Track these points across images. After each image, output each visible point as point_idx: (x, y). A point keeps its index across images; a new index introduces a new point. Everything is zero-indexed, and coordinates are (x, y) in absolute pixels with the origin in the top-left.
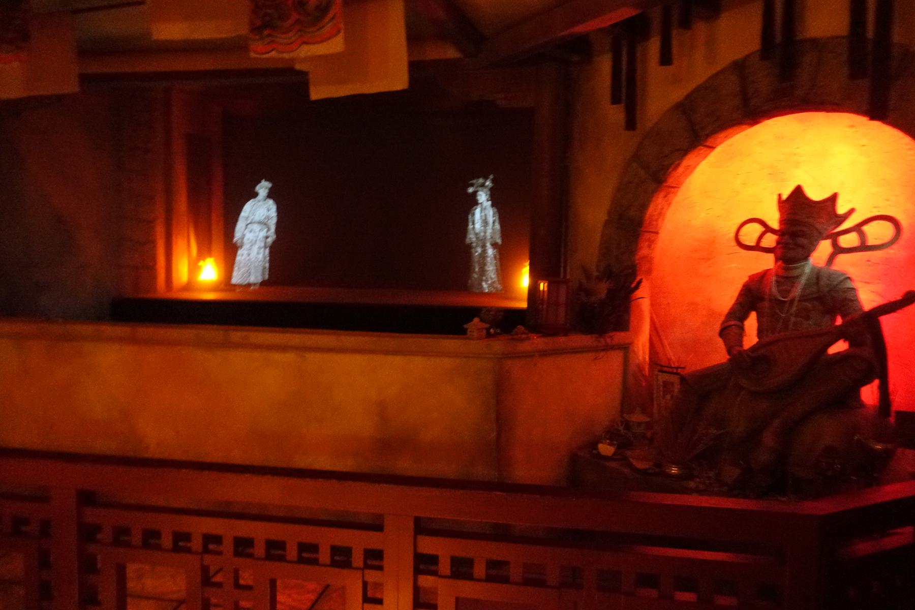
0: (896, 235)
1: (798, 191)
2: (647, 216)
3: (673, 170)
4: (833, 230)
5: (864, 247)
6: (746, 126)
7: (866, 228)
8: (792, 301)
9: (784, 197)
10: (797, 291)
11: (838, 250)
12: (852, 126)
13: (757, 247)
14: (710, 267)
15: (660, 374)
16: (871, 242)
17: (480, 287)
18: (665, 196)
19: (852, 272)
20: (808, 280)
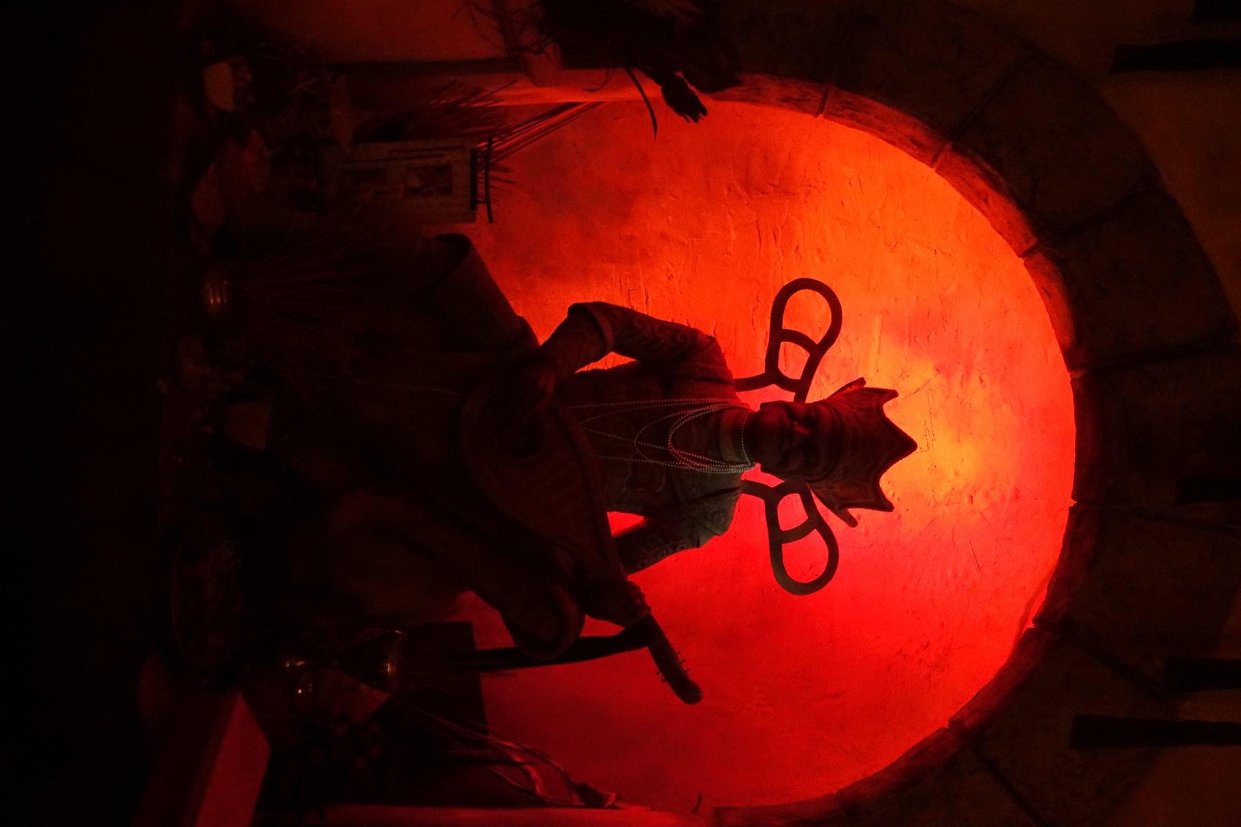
0: (797, 584)
1: (905, 446)
2: (869, 102)
3: (982, 169)
4: (818, 496)
5: (778, 538)
6: (1067, 340)
7: (815, 535)
8: (668, 456)
9: (891, 411)
10: (688, 463)
11: (772, 498)
12: (1017, 496)
13: (779, 334)
14: (730, 190)
15: (468, 156)
16: (787, 548)
17: (824, 410)
18: (913, 140)
19: (735, 526)
20: (714, 477)
